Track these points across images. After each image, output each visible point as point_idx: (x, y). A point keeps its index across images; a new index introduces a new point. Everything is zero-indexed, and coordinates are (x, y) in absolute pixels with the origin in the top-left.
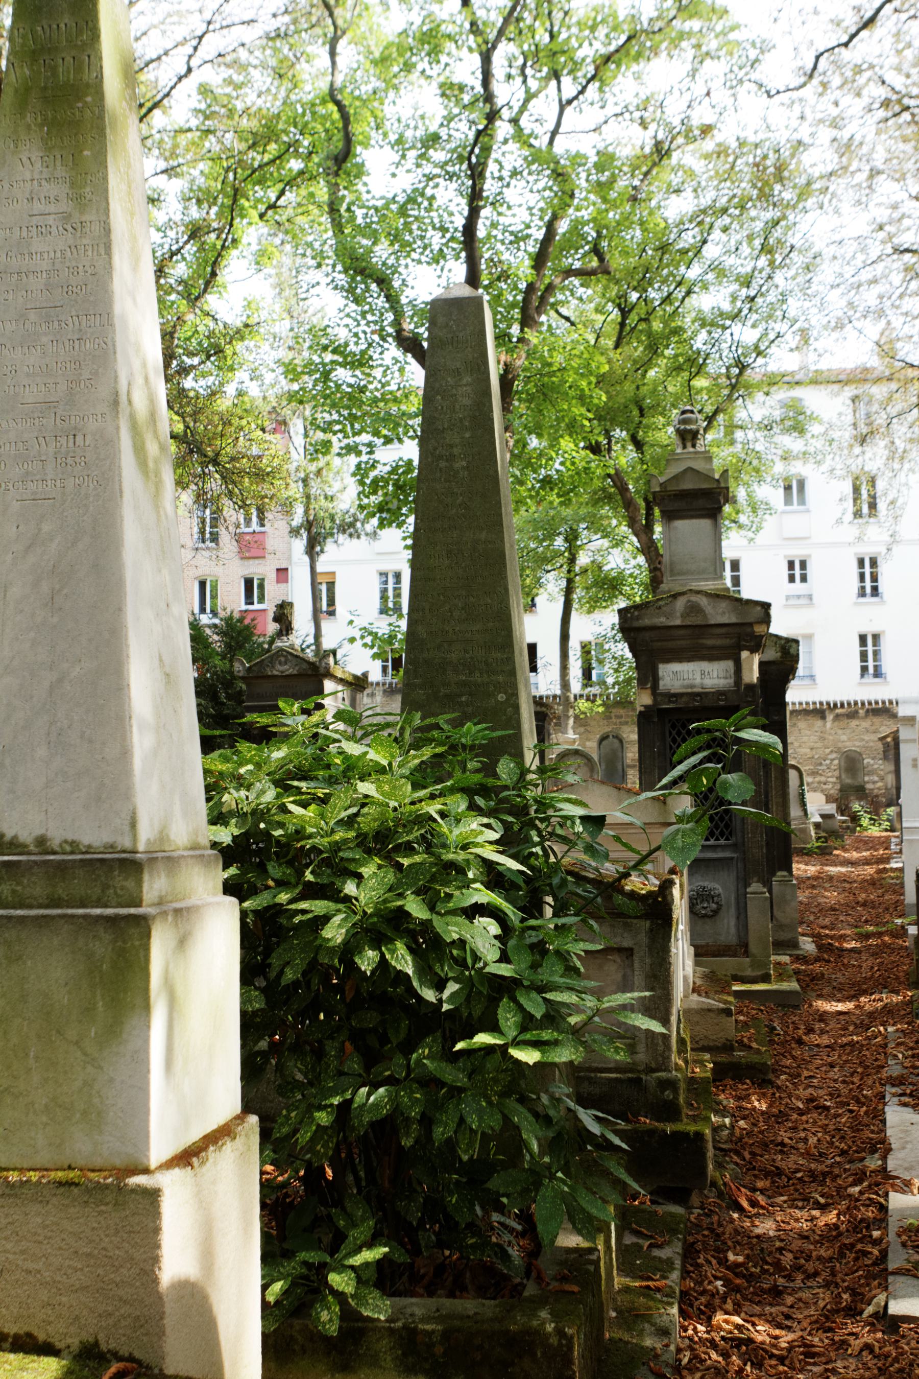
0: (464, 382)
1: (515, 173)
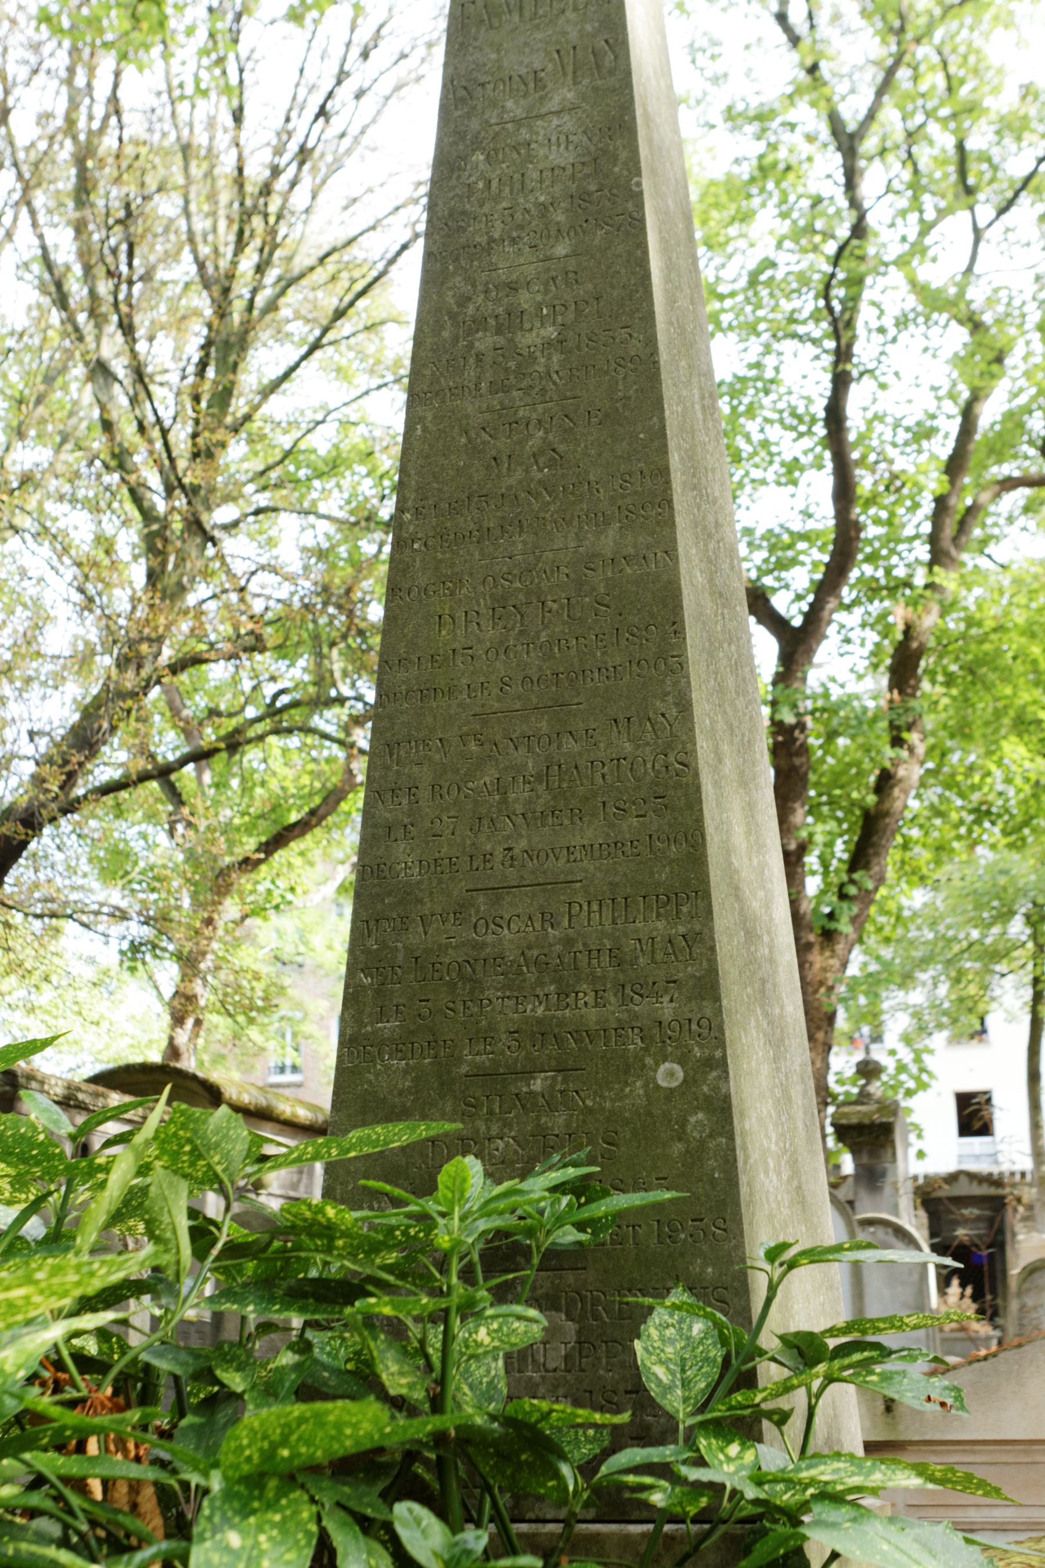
0: (554, 104)
1: (902, 322)
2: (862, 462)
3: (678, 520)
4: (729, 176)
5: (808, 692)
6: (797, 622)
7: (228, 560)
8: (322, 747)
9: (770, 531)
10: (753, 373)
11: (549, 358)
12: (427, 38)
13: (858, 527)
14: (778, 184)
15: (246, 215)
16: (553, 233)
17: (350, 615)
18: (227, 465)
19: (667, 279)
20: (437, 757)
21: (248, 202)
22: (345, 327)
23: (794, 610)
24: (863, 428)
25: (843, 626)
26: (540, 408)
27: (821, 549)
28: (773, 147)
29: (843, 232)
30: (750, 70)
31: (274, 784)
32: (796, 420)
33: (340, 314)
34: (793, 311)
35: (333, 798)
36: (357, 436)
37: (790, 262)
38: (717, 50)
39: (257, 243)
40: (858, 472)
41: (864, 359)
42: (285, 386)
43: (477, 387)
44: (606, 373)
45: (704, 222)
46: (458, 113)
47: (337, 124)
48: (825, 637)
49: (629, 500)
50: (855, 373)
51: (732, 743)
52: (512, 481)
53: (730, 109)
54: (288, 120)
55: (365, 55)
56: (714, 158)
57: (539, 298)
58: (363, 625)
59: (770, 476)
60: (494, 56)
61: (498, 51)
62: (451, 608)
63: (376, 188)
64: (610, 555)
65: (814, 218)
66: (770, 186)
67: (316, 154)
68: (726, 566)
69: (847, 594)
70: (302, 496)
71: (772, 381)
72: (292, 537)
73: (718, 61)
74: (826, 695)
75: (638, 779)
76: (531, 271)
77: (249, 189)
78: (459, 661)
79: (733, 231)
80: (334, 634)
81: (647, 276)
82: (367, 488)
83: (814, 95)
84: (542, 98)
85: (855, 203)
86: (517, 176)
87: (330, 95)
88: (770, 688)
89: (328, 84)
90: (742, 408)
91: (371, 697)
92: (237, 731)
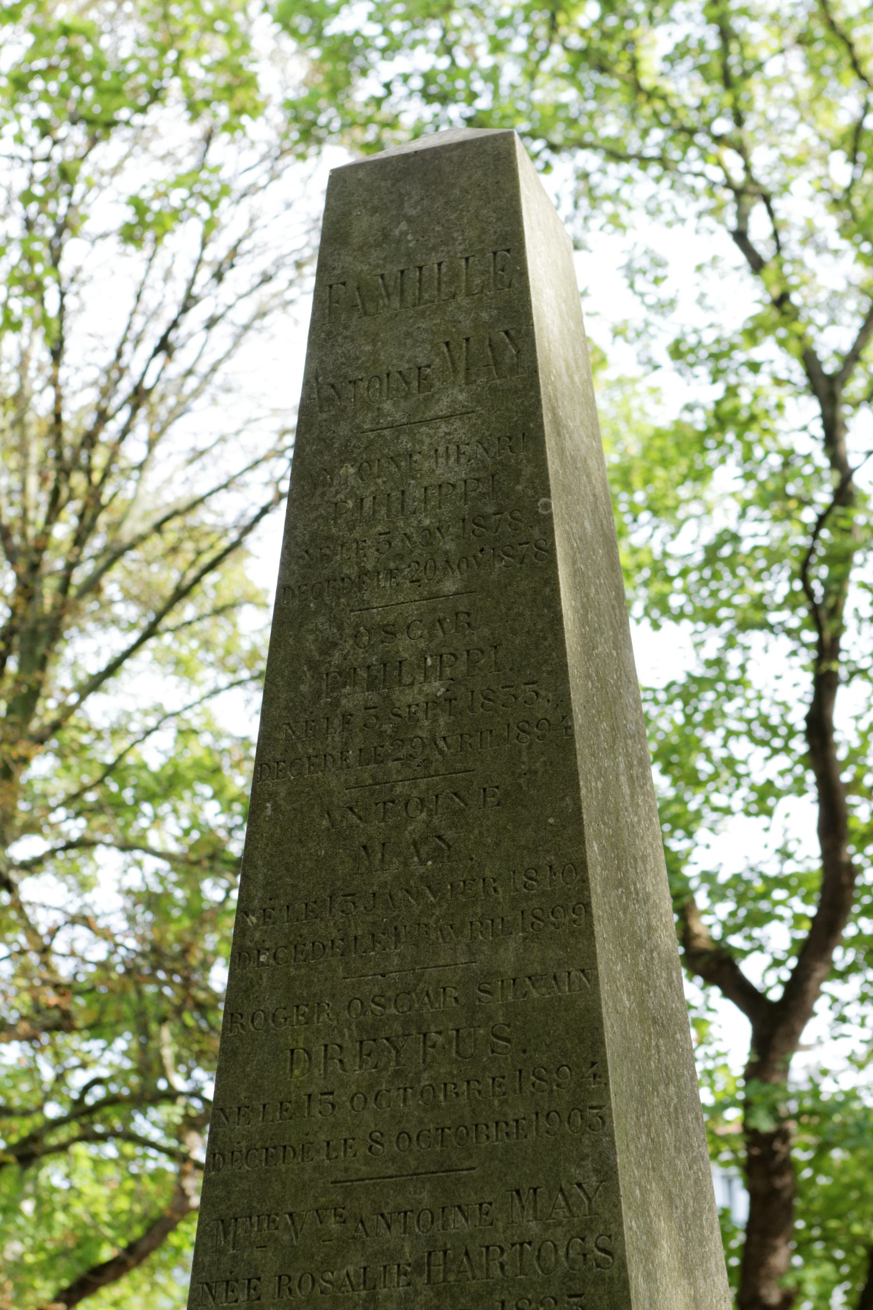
0: (442, 406)
2: (855, 785)
3: (598, 928)
4: (678, 423)
5: (791, 1089)
6: (776, 994)
7: (28, 910)
8: (145, 1157)
9: (737, 877)
10: (712, 673)
11: (435, 721)
12: (295, 257)
13: (853, 871)
14: (739, 436)
15: (65, 472)
16: (440, 564)
17: (187, 983)
18: (30, 783)
19: (584, 621)
20: (286, 1237)
21: (67, 453)
22: (188, 610)
23: (771, 978)
24: (856, 743)
25: (835, 1000)
26: (423, 783)
27: (806, 900)
28: (732, 391)
29: (824, 497)
30: (703, 296)
31: (78, 1208)
32: (766, 732)
33: (181, 593)
34: (762, 595)
35: (159, 1228)
36: (198, 747)
37: (758, 532)
38: (660, 272)
39: (76, 505)
40: (852, 799)
41: (854, 656)
42: (109, 682)
43: (344, 757)
44: (506, 740)
45: (647, 482)
46: (325, 416)
47: (183, 359)
48: (814, 1014)
49: (534, 903)
50: (843, 673)
51: (670, 1218)
52: (387, 876)
53: (678, 343)
54: (119, 355)
55: (219, 276)
56: (658, 402)
57: (422, 645)
58: (201, 996)
59: (737, 804)
60: (368, 348)
61: (374, 342)
62: (306, 1039)
63: (231, 435)
64: (511, 974)
65: (786, 480)
66: (730, 437)
67: (154, 397)
68: (661, 982)
69: (841, 957)
70: (128, 825)
71: (737, 683)
72: (113, 879)
73: (664, 285)
74: (815, 1092)
75: (546, 1271)
76: (412, 611)
77: (68, 436)
78: (316, 1109)
79: (684, 492)
80: (166, 1007)
81: (557, 619)
82: (213, 814)
83: (782, 332)
84: (427, 399)
85: (838, 462)
86: (396, 494)
87: (175, 324)
88: (742, 1083)
89: (171, 312)
90: (698, 717)
91: (209, 1092)
92: (34, 1138)
